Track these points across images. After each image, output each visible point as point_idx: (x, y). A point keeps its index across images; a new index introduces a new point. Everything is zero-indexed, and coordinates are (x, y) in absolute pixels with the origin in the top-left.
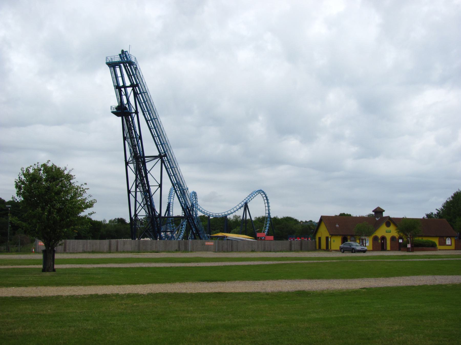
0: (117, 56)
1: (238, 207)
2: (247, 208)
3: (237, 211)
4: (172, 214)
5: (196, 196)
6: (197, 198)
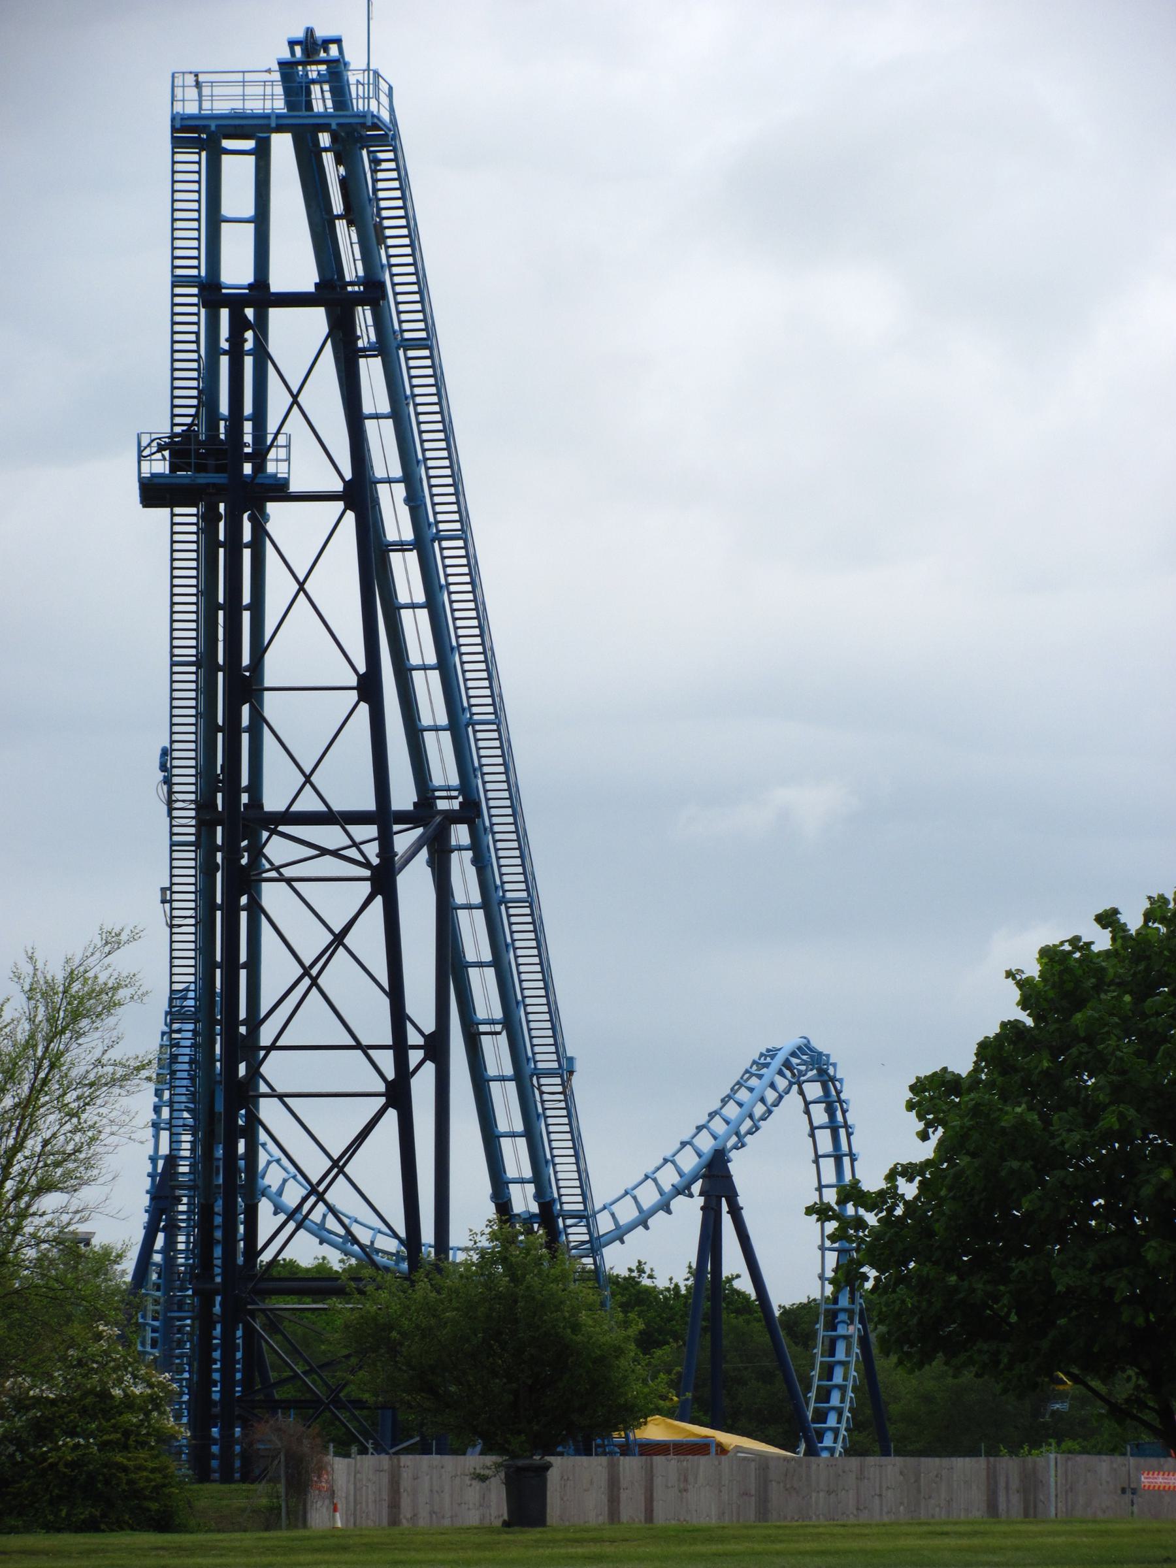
0: (269, 71)
1: (649, 1196)
2: (725, 1207)
4: (366, 312)
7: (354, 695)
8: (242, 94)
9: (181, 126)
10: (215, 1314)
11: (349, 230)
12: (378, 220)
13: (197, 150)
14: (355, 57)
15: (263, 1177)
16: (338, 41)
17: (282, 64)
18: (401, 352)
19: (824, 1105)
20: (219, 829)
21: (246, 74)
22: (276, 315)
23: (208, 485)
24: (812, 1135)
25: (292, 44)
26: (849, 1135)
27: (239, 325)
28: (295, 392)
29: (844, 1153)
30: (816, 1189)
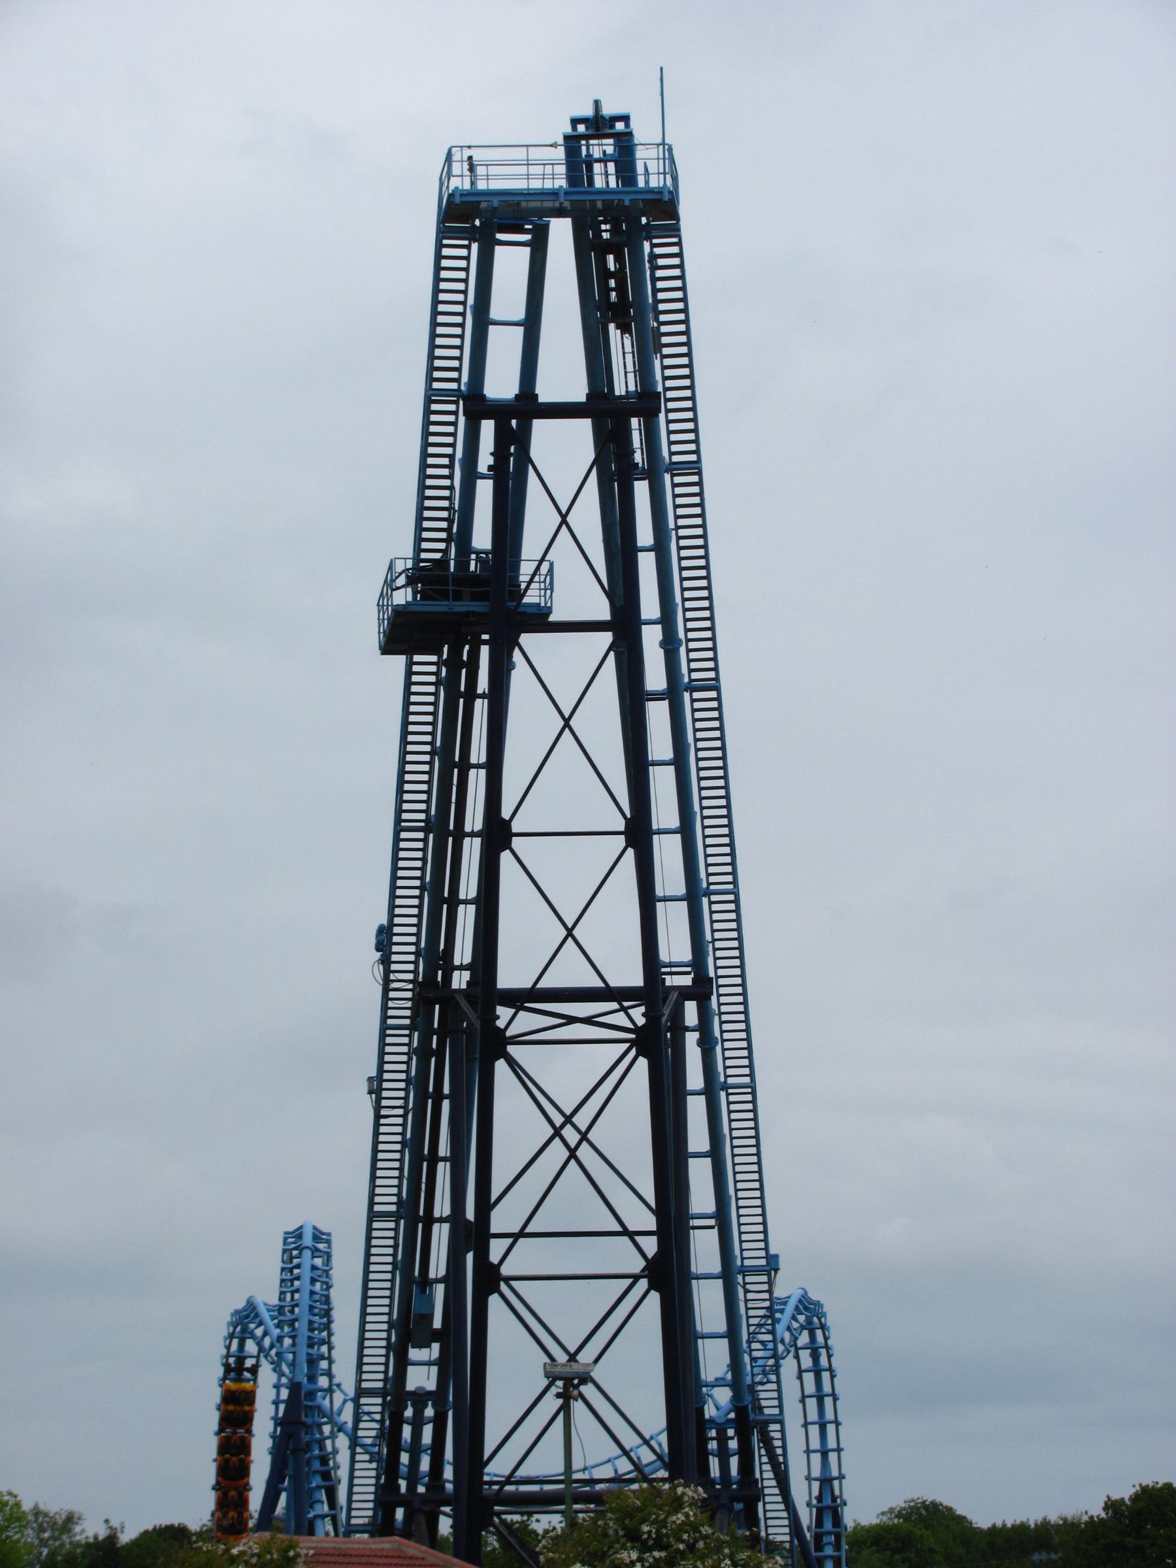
0: (554, 145)
3: (582, 1472)
5: (823, 1327)
6: (827, 1347)
7: (621, 841)
8: (526, 173)
9: (461, 202)
10: (397, 1529)
11: (622, 338)
12: (655, 325)
13: (466, 242)
14: (644, 131)
15: (339, 1414)
16: (626, 119)
17: (567, 138)
18: (667, 477)
19: (809, 1350)
20: (437, 1007)
21: (530, 148)
22: (540, 427)
23: (467, 613)
24: (800, 1378)
25: (575, 122)
26: (833, 1377)
27: (503, 438)
28: (564, 512)
29: (825, 1393)
30: (803, 1426)
